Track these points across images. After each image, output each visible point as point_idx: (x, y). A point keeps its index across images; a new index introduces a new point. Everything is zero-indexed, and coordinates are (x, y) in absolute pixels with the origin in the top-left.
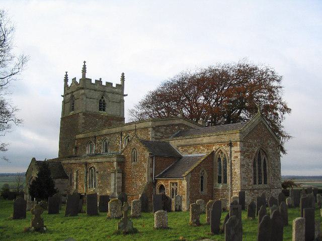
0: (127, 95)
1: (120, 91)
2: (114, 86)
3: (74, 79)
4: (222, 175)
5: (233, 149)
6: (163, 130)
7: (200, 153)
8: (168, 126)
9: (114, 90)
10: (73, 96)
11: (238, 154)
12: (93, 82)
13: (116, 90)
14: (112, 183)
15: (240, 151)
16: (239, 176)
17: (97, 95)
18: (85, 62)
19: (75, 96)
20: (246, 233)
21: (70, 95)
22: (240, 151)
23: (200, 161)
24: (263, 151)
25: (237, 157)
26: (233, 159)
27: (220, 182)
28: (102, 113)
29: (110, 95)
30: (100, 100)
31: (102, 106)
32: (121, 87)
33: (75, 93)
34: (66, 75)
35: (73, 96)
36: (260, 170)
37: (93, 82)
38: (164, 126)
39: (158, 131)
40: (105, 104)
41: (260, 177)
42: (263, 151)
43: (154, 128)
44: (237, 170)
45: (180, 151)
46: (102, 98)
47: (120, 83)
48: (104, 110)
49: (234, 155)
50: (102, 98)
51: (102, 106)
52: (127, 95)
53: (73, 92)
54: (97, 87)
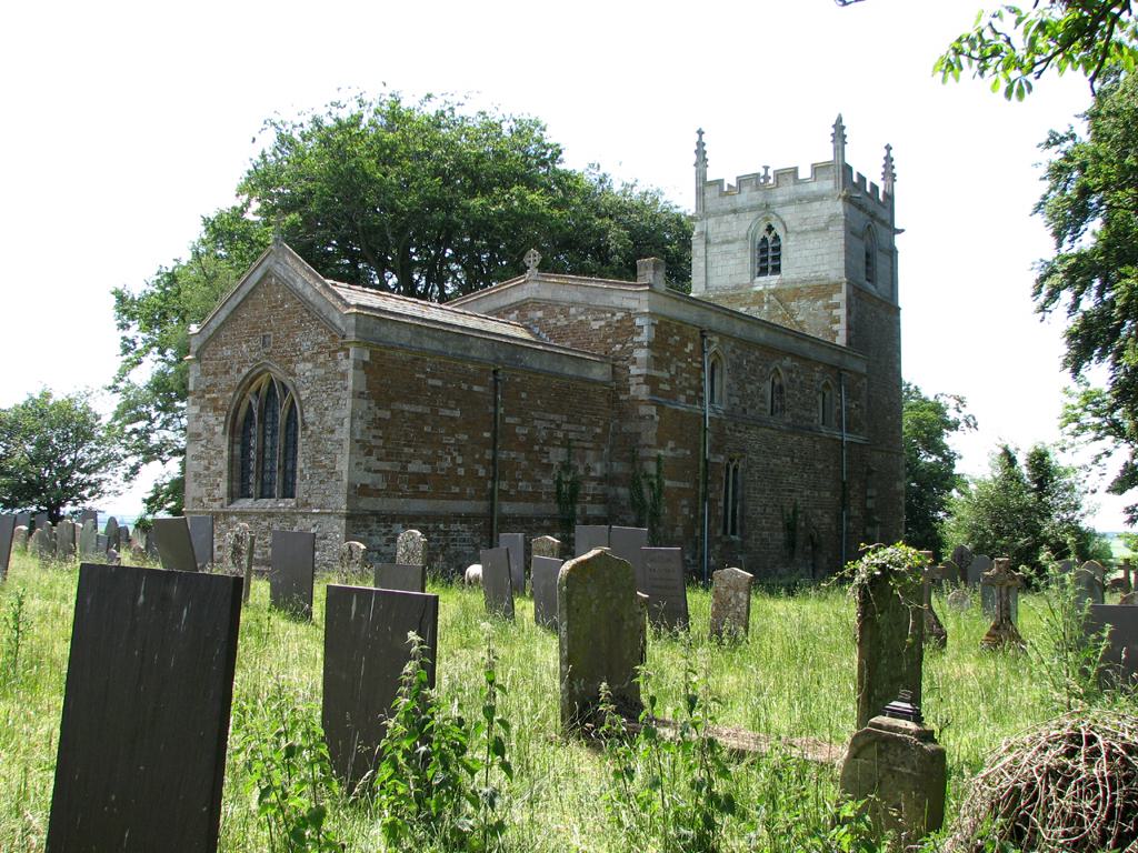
29: (790, 214)
34: (701, 144)
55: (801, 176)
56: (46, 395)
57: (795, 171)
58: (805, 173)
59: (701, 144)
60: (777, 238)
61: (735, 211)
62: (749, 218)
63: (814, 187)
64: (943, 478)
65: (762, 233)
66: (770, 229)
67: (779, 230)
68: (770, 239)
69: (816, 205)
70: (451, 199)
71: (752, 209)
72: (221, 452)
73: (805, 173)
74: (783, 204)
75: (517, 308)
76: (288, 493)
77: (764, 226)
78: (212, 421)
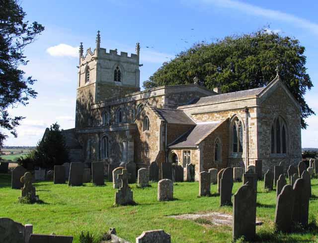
0: (142, 65)
7: (215, 120)
10: (88, 68)
17: (112, 65)
18: (81, 43)
21: (85, 66)
28: (117, 83)
29: (125, 65)
31: (118, 76)
32: (136, 57)
34: (99, 35)
35: (88, 68)
38: (178, 94)
47: (135, 53)
48: (119, 81)
52: (142, 65)
53: (88, 63)
54: (112, 57)
55: (128, 56)
56: (56, 126)
57: (127, 54)
58: (129, 55)
59: (99, 35)
60: (119, 71)
61: (110, 60)
62: (113, 63)
63: (131, 60)
64: (149, 160)
65: (115, 69)
66: (117, 68)
67: (120, 69)
68: (117, 71)
69: (132, 65)
70: (218, 67)
71: (115, 61)
72: (269, 139)
73: (129, 55)
74: (124, 62)
75: (192, 93)
76: (284, 152)
77: (116, 66)
78: (265, 128)
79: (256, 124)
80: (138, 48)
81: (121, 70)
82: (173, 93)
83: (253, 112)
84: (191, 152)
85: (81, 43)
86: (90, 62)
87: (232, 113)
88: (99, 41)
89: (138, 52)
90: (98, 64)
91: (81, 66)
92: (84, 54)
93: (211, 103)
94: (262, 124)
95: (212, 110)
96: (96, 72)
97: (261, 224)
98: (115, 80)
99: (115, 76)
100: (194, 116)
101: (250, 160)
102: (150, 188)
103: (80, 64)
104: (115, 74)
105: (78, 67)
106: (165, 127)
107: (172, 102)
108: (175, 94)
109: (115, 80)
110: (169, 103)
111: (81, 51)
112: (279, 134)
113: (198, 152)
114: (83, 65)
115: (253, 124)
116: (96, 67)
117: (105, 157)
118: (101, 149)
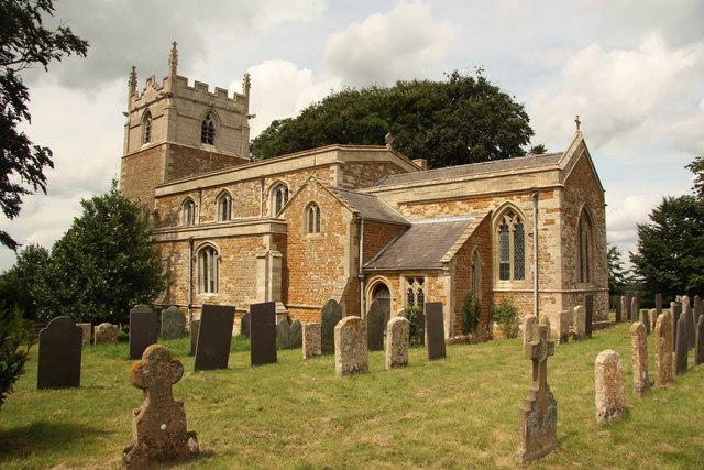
0: (254, 116)
1: (241, 108)
2: (231, 96)
3: (11, 172)
4: (511, 262)
5: (541, 203)
6: (357, 171)
7: (457, 215)
8: (366, 164)
9: (230, 104)
10: (148, 114)
11: (556, 216)
12: (191, 84)
13: (235, 105)
14: (261, 279)
15: (561, 210)
16: (558, 263)
17: (199, 112)
18: (175, 44)
19: (154, 114)
20: (247, 349)
21: (141, 112)
22: (561, 210)
23: (464, 237)
24: (587, 215)
25: (552, 222)
26: (541, 226)
27: (504, 276)
28: (207, 148)
29: (222, 114)
30: (204, 123)
31: (208, 134)
32: (243, 99)
33: (151, 107)
34: (174, 52)
35: (148, 114)
36: (212, 276)
37: (191, 84)
38: (360, 163)
39: (348, 173)
40: (212, 130)
41: (206, 285)
42: (587, 215)
43: (342, 167)
44: (555, 251)
45: (406, 215)
46: (208, 118)
47: (241, 91)
48: (211, 142)
49: (543, 216)
50: (208, 118)
51: (208, 134)
52: (254, 116)
53: (147, 105)
54: (197, 96)
60: (211, 124)
79: (558, 222)
80: (248, 86)
81: (214, 122)
82: (352, 162)
83: (552, 197)
84: (426, 279)
85: (175, 44)
86: (153, 103)
87: (501, 201)
88: (174, 63)
89: (248, 91)
90: (173, 110)
91: (132, 112)
92: (140, 89)
93: (447, 181)
94: (566, 222)
95: (455, 194)
96: (167, 121)
97: (90, 367)
98: (203, 140)
99: (203, 134)
100: (402, 207)
101: (542, 296)
102: (407, 368)
103: (130, 106)
104: (204, 129)
105: (126, 114)
106: (359, 227)
107: (350, 178)
108: (356, 163)
109: (203, 140)
110: (345, 181)
111: (133, 84)
112: (516, 253)
113: (445, 281)
114: (137, 110)
115: (552, 222)
116: (167, 112)
117: (206, 291)
118: (196, 276)
